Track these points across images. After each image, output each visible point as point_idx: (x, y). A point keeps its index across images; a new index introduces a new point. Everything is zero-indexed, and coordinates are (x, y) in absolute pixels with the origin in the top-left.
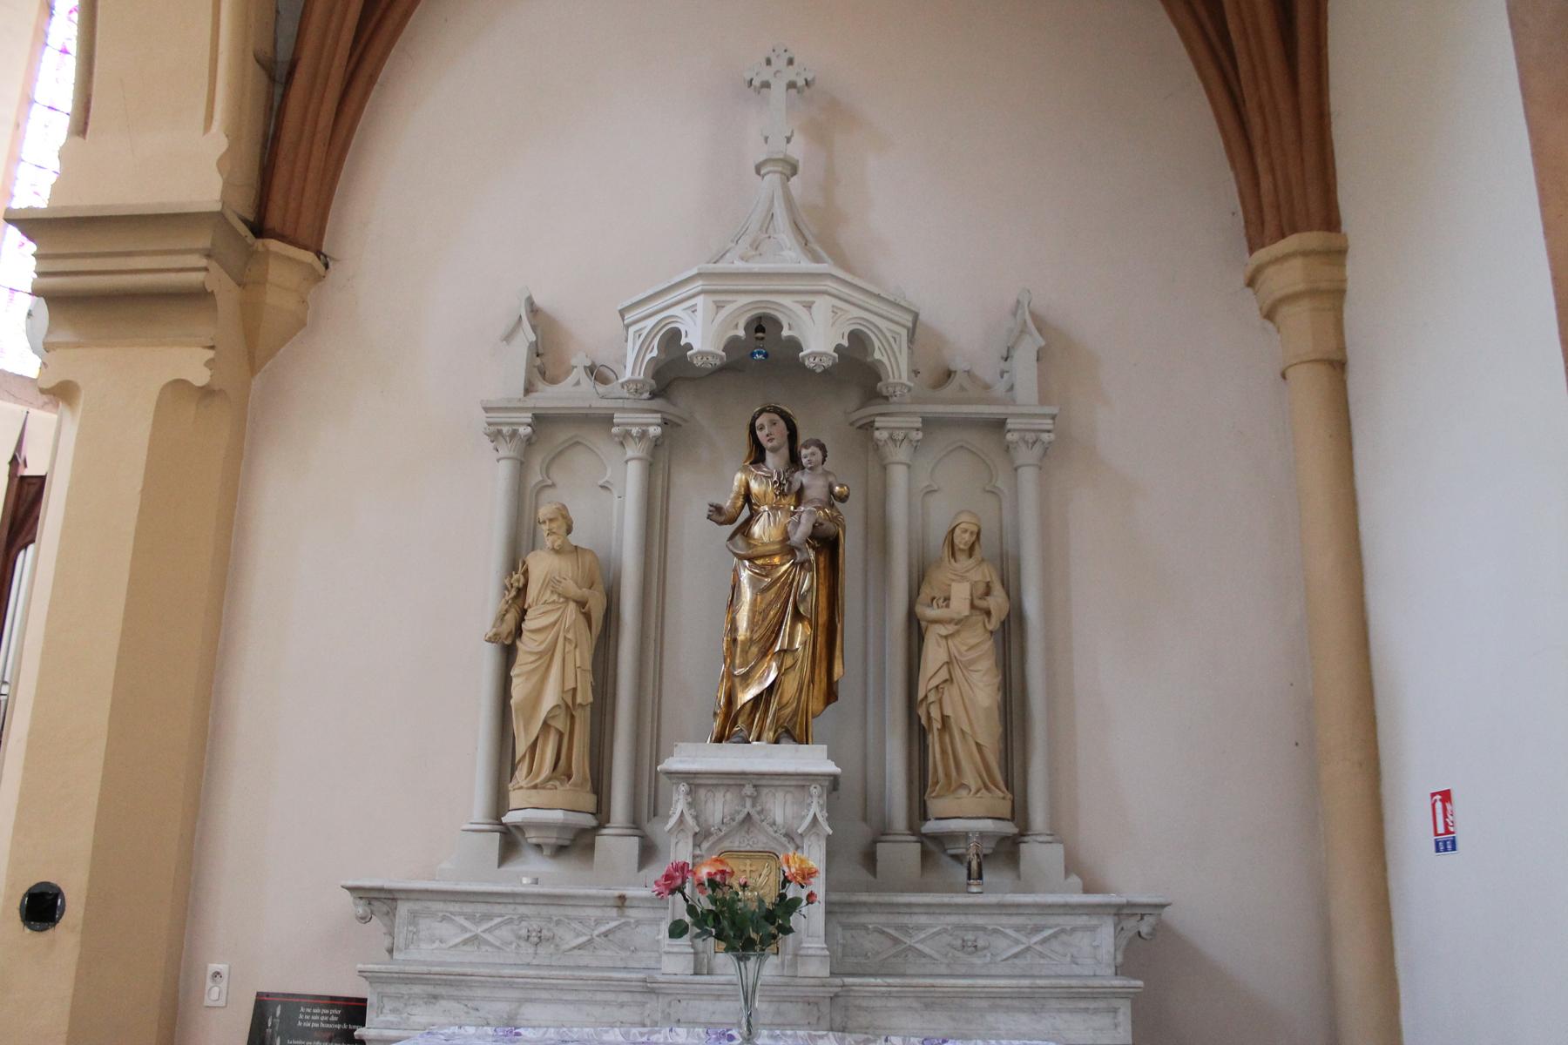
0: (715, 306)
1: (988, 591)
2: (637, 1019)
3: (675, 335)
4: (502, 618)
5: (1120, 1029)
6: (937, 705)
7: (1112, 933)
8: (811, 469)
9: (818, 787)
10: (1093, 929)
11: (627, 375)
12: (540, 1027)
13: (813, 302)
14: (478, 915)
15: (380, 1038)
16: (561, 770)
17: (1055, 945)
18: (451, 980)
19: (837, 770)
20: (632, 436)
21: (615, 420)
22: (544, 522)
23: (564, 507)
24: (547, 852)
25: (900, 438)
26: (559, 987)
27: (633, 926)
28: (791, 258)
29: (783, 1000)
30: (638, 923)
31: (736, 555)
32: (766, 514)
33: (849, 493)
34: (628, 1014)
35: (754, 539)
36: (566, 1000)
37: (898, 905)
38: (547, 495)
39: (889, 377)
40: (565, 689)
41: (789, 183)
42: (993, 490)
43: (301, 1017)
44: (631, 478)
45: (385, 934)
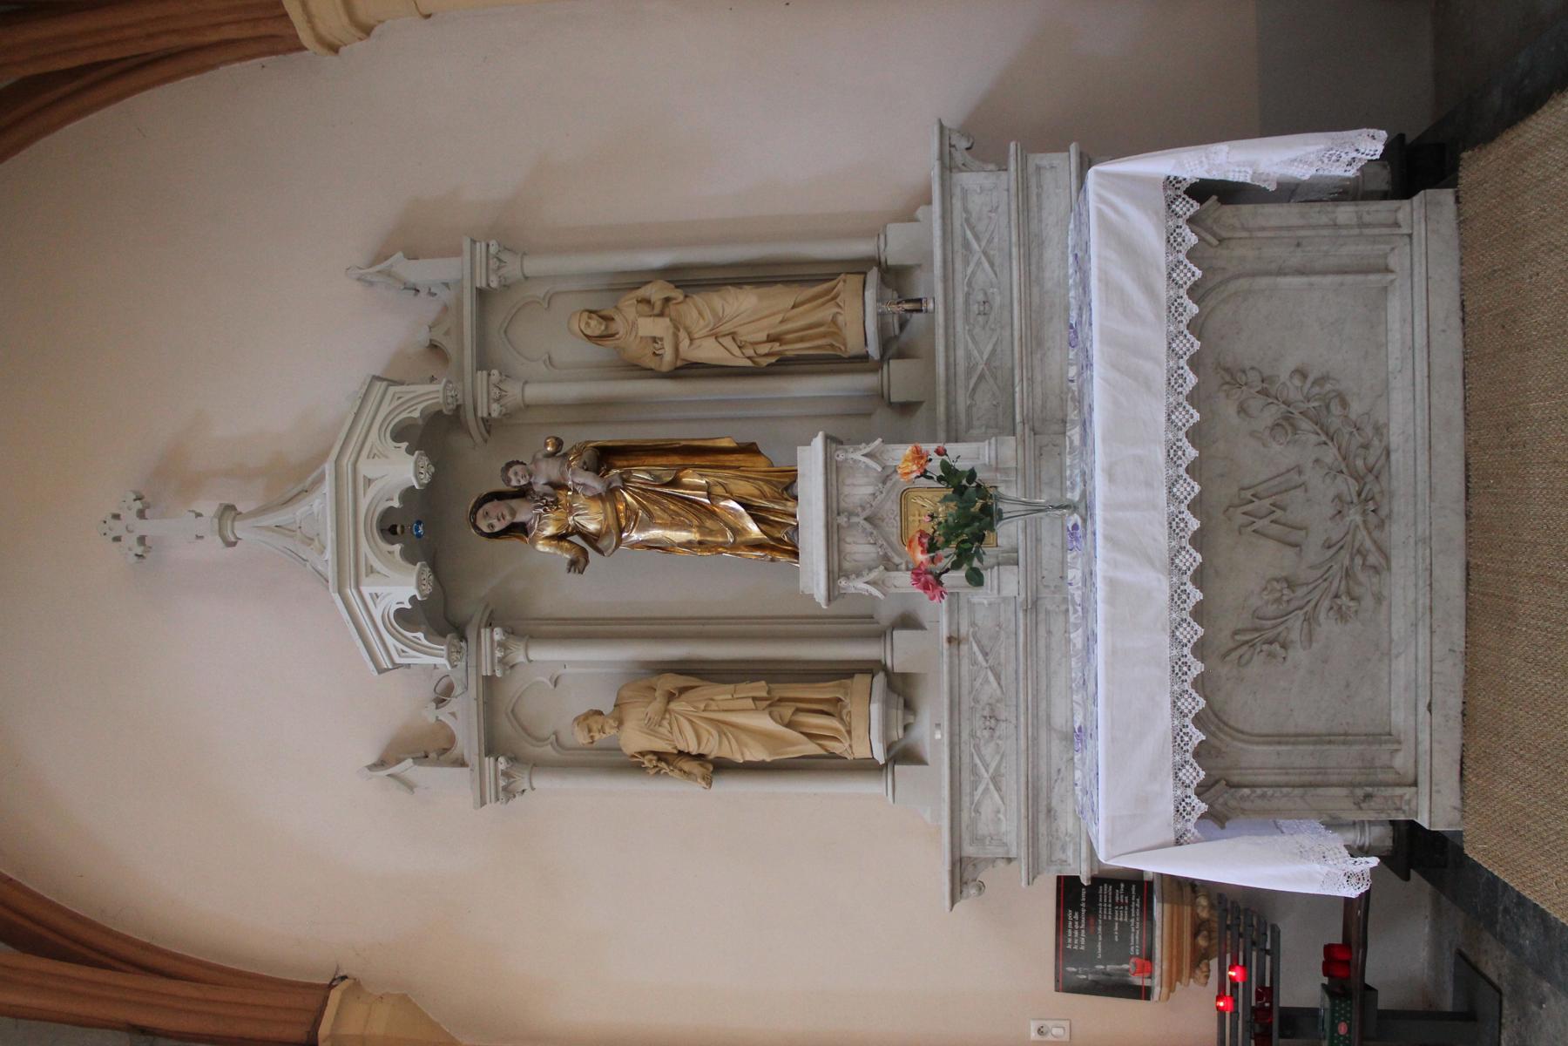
0: (372, 575)
1: (647, 301)
2: (1061, 618)
3: (401, 615)
4: (687, 774)
5: (1055, 163)
6: (757, 347)
7: (969, 174)
8: (531, 476)
9: (838, 452)
10: (965, 192)
11: (442, 661)
12: (1072, 709)
13: (364, 476)
14: (972, 778)
15: (1089, 861)
16: (832, 708)
17: (981, 227)
18: (1033, 794)
19: (821, 434)
20: (504, 657)
21: (489, 674)
22: (592, 737)
23: (576, 719)
24: (911, 719)
25: (498, 391)
26: (1035, 693)
27: (977, 628)
28: (320, 503)
29: (1038, 477)
30: (973, 624)
31: (617, 546)
32: (576, 518)
33: (553, 437)
34: (1057, 626)
35: (601, 529)
36: (1047, 686)
37: (947, 376)
38: (567, 739)
39: (438, 403)
40: (753, 707)
41: (243, 512)
42: (547, 301)
43: (1076, 947)
44: (545, 654)
45: (993, 867)
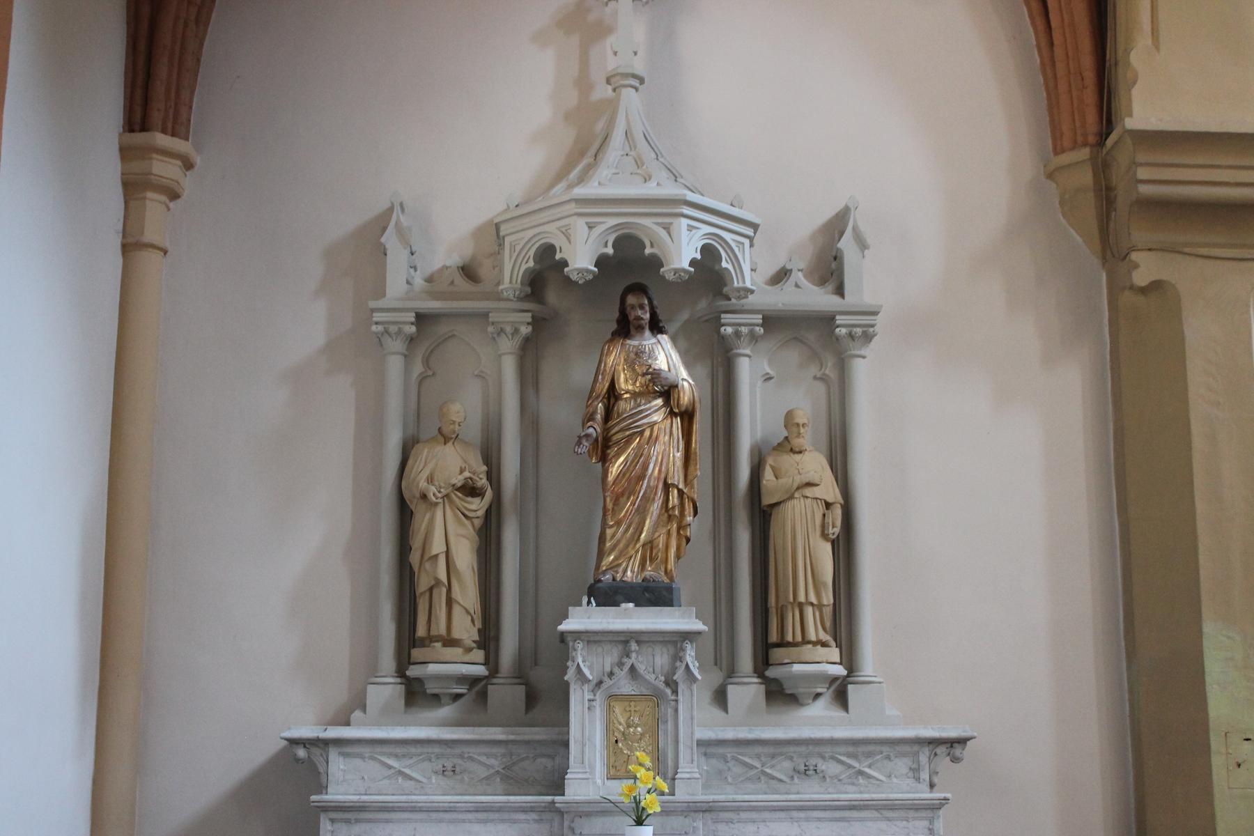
13: (671, 223)
